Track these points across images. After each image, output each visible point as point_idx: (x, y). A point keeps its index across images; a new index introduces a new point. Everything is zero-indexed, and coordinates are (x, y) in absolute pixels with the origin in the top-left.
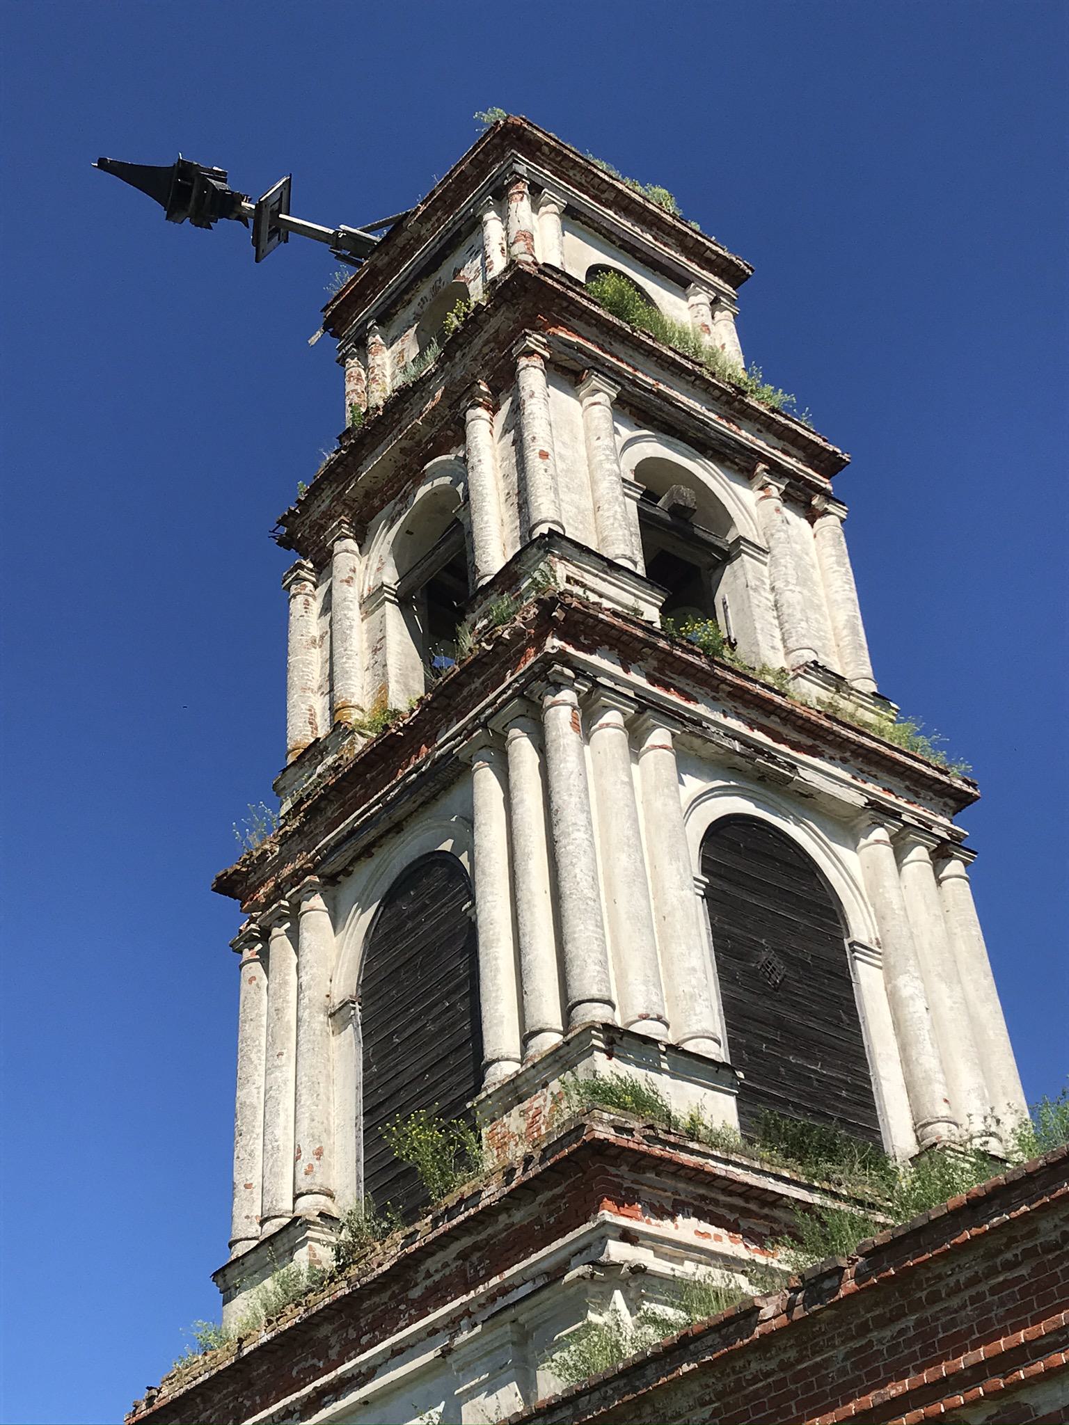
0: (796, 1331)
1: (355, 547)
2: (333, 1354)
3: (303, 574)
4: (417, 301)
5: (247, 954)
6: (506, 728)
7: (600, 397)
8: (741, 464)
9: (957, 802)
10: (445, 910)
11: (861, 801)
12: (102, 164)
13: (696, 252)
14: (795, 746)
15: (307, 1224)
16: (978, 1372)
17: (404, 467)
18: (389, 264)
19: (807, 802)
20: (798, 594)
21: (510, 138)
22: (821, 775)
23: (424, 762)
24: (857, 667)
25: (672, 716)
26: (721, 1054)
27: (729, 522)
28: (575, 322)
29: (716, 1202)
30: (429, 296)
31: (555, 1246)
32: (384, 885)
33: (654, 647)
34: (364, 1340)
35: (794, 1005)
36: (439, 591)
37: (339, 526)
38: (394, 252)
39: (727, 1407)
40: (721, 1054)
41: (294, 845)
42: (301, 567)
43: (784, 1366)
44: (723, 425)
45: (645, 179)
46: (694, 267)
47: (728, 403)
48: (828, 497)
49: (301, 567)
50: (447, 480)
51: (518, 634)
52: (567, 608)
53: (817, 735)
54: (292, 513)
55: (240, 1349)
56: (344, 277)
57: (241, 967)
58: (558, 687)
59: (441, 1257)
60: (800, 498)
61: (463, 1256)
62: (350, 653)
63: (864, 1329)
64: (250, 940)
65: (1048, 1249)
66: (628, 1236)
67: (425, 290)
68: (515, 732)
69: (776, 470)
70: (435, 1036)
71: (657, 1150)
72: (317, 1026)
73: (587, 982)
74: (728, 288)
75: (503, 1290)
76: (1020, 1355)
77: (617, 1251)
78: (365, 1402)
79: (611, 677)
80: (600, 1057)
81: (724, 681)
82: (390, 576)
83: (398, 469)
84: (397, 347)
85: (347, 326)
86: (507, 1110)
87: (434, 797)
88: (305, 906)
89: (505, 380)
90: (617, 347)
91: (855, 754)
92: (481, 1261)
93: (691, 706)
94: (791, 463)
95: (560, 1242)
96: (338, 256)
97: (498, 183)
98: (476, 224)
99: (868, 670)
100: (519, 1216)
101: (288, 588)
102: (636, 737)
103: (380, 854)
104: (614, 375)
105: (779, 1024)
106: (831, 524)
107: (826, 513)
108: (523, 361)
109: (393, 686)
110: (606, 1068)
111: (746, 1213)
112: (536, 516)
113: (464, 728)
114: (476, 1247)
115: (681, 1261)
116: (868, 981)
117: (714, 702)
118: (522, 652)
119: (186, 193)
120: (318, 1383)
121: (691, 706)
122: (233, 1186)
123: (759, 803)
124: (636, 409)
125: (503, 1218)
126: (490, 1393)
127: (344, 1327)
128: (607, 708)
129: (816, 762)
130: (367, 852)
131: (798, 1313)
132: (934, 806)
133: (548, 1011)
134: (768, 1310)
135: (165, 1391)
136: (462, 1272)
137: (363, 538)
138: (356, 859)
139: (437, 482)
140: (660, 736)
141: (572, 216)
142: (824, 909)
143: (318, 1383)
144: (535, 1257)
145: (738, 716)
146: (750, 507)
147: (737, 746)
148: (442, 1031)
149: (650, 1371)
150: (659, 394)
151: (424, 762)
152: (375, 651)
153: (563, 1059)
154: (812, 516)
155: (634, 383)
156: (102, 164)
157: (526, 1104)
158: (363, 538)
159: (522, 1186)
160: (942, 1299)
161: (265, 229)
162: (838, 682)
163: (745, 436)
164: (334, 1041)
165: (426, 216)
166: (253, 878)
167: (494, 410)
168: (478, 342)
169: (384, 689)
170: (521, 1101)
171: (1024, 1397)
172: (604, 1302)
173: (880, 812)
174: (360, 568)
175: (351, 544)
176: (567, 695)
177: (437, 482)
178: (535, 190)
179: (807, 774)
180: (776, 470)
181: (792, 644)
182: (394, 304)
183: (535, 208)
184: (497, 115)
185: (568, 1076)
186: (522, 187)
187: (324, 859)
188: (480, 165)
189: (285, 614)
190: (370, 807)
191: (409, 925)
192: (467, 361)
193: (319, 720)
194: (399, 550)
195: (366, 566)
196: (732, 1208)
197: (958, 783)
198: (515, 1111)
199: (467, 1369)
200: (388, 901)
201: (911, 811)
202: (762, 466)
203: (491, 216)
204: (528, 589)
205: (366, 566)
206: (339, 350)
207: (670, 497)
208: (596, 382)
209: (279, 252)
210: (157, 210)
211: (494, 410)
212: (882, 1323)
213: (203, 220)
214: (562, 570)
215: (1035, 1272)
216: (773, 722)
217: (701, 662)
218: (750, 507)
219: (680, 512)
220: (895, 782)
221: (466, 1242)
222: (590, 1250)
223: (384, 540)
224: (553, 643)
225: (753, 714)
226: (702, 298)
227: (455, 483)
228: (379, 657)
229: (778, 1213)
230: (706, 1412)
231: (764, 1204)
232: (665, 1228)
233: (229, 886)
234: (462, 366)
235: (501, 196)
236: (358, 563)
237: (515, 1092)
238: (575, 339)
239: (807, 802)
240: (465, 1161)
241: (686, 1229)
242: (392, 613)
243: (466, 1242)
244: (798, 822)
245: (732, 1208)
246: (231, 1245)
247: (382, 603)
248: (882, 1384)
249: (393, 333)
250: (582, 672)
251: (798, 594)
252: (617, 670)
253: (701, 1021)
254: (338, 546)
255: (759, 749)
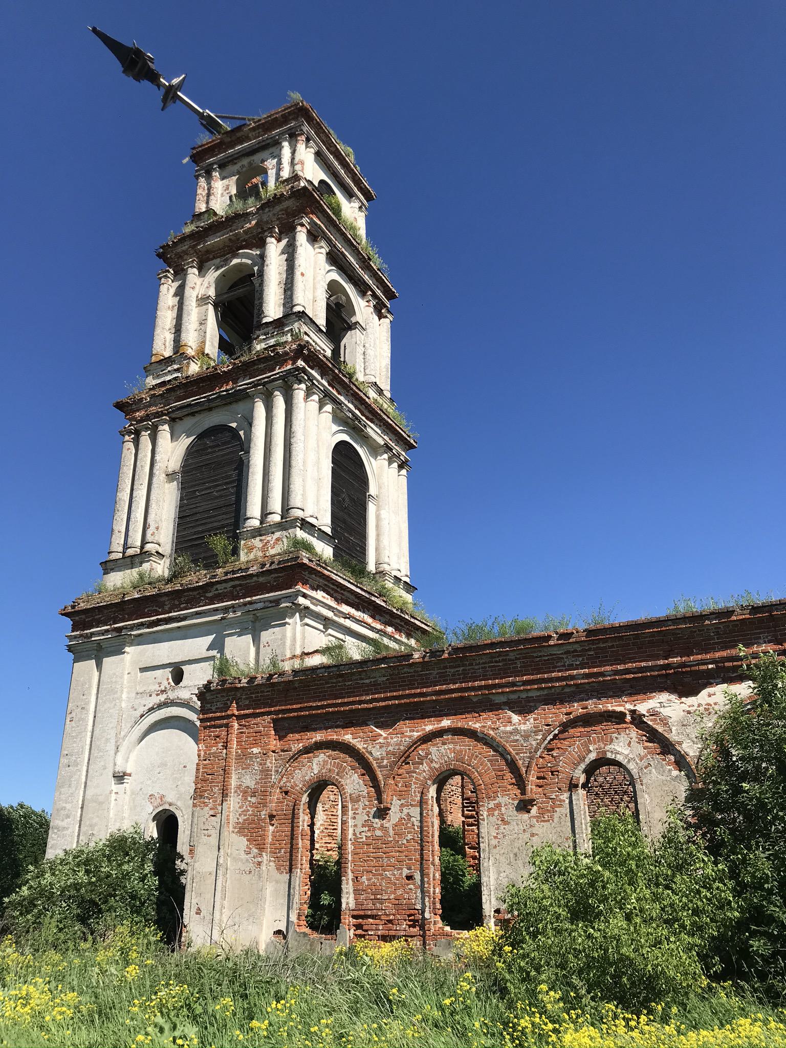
0: (423, 664)
1: (197, 273)
2: (166, 608)
3: (169, 275)
4: (240, 164)
5: (127, 438)
6: (274, 390)
7: (323, 251)
8: (363, 289)
9: (409, 446)
10: (231, 449)
11: (382, 443)
12: (94, 30)
13: (358, 183)
14: (367, 418)
15: (151, 555)
16: (480, 688)
17: (228, 246)
18: (230, 142)
19: (365, 439)
20: (371, 350)
21: (301, 112)
22: (374, 431)
23: (231, 389)
24: (386, 386)
25: (334, 401)
26: (328, 530)
27: (354, 313)
28: (319, 214)
29: (329, 587)
30: (246, 165)
31: (277, 593)
32: (200, 431)
33: (334, 371)
34: (182, 606)
35: (349, 515)
36: (238, 308)
37: (192, 262)
38: (234, 138)
39: (392, 679)
40: (328, 530)
41: (158, 400)
42: (168, 271)
43: (415, 672)
44: (361, 272)
45: (346, 142)
46: (355, 189)
47: (364, 262)
48: (389, 312)
49: (168, 271)
50: (250, 262)
51: (286, 353)
52: (309, 350)
53: (375, 415)
54: (168, 245)
55: (123, 597)
56: (205, 138)
57: (123, 442)
58: (300, 382)
59: (224, 585)
60: (379, 310)
61: (234, 587)
62: (186, 320)
63: (446, 667)
64: (129, 433)
65: (510, 660)
66: (305, 596)
67: (245, 161)
68: (277, 393)
69: (374, 295)
70: (217, 498)
71: (319, 569)
72: (161, 478)
73: (296, 500)
74: (365, 202)
75: (250, 603)
76: (495, 686)
77: (301, 600)
78: (179, 627)
79: (318, 381)
80: (298, 529)
81: (352, 389)
82: (212, 292)
83: (225, 246)
84: (226, 182)
85: (204, 161)
86: (254, 537)
87: (230, 403)
88: (160, 428)
89: (288, 230)
90: (331, 229)
91: (384, 424)
92: (241, 590)
93: (339, 396)
94: (379, 293)
95: (280, 593)
96: (202, 124)
97: (293, 131)
98: (277, 144)
99: (389, 388)
100: (261, 579)
101: (160, 279)
102: (321, 405)
103: (197, 418)
104: (329, 241)
105: (344, 522)
106: (386, 322)
107: (386, 317)
108: (299, 228)
109: (208, 343)
110: (300, 534)
111: (336, 591)
112: (296, 301)
113: (253, 382)
114: (240, 585)
115: (316, 605)
116: (371, 508)
117: (346, 396)
118: (286, 361)
119: (135, 64)
120: (159, 617)
121: (339, 396)
122: (112, 530)
123: (352, 438)
124: (334, 259)
125: (255, 579)
126: (239, 636)
127: (174, 599)
128: (314, 393)
129: (372, 425)
130: (193, 414)
131: (427, 659)
132: (402, 448)
133: (276, 504)
134: (416, 656)
135: (82, 605)
136: (231, 592)
137: (202, 270)
138: (188, 415)
139: (244, 260)
140: (329, 408)
141: (319, 155)
142: (362, 480)
143: (159, 617)
144: (267, 595)
145: (353, 403)
146: (363, 309)
147: (350, 415)
148: (221, 496)
149: (369, 664)
150: (342, 253)
151: (231, 389)
152: (201, 324)
153: (281, 526)
154: (380, 316)
155: (334, 246)
156: (94, 30)
157: (263, 538)
158: (202, 270)
159: (267, 571)
160: (625, 722)
161: (171, 96)
162: (380, 392)
163: (366, 277)
164: (167, 485)
165: (253, 129)
166: (134, 407)
167: (279, 240)
168: (278, 208)
169: (204, 342)
170: (261, 535)
171: (491, 696)
172: (292, 616)
173: (388, 448)
174: (199, 283)
175: (196, 271)
176: (303, 386)
177: (244, 260)
178: (308, 140)
179: (369, 430)
180: (374, 295)
181: (368, 372)
182: (229, 162)
183: (307, 147)
184: (296, 96)
185: (285, 533)
186: (303, 138)
187: (173, 411)
188: (285, 119)
189: (158, 292)
190: (202, 398)
191: (209, 450)
192: (271, 214)
193: (167, 344)
194: (218, 282)
195: (202, 284)
196: (333, 589)
197: (412, 441)
198: (258, 539)
199: (231, 625)
200: (200, 437)
201: (397, 449)
202: (370, 293)
203: (286, 144)
204: (288, 331)
205: (202, 284)
206: (197, 171)
207: (337, 298)
208: (323, 243)
209: (172, 107)
210: (117, 66)
211: (279, 240)
212: (451, 667)
213: (138, 78)
214: (304, 328)
215: (504, 665)
216: (362, 408)
217: (346, 380)
218: (363, 309)
219: (338, 305)
220: (393, 437)
221: (237, 582)
222: (292, 598)
223: (213, 275)
224: (300, 363)
225: (357, 403)
226: (356, 205)
227: (254, 264)
228: (202, 327)
229: (345, 593)
230: (385, 679)
231: (342, 589)
232: (313, 593)
233: (120, 406)
234: (267, 215)
235: (293, 136)
236: (199, 281)
237: (258, 532)
238: (319, 222)
239: (365, 439)
240: (235, 552)
241: (320, 595)
242: (211, 308)
243: (237, 582)
244: (361, 447)
245: (333, 589)
246: (109, 553)
247: (207, 304)
248: (448, 684)
249: (224, 174)
250: (311, 379)
251: (371, 350)
252: (319, 378)
253: (325, 521)
254: (190, 270)
255: (357, 418)
